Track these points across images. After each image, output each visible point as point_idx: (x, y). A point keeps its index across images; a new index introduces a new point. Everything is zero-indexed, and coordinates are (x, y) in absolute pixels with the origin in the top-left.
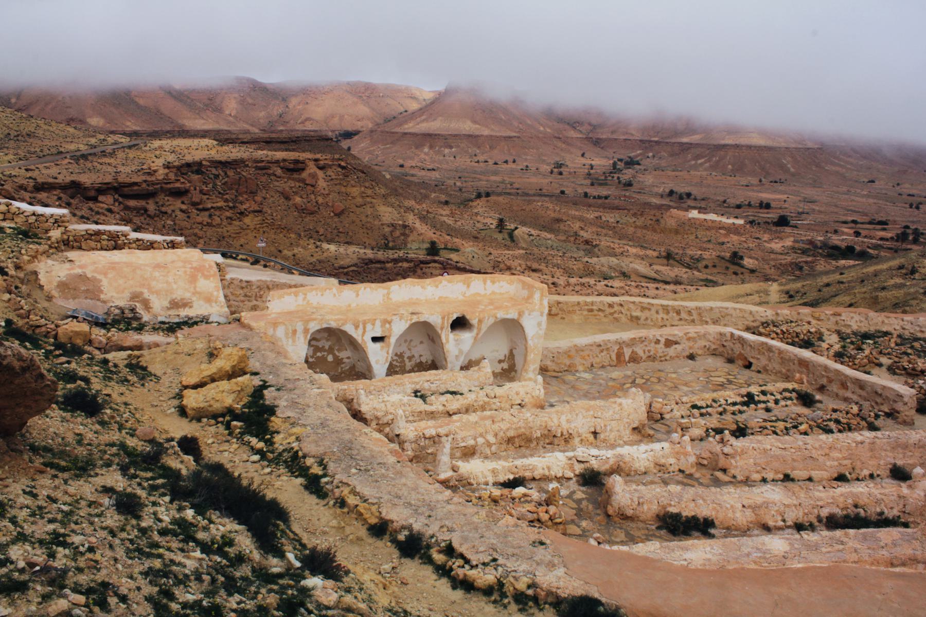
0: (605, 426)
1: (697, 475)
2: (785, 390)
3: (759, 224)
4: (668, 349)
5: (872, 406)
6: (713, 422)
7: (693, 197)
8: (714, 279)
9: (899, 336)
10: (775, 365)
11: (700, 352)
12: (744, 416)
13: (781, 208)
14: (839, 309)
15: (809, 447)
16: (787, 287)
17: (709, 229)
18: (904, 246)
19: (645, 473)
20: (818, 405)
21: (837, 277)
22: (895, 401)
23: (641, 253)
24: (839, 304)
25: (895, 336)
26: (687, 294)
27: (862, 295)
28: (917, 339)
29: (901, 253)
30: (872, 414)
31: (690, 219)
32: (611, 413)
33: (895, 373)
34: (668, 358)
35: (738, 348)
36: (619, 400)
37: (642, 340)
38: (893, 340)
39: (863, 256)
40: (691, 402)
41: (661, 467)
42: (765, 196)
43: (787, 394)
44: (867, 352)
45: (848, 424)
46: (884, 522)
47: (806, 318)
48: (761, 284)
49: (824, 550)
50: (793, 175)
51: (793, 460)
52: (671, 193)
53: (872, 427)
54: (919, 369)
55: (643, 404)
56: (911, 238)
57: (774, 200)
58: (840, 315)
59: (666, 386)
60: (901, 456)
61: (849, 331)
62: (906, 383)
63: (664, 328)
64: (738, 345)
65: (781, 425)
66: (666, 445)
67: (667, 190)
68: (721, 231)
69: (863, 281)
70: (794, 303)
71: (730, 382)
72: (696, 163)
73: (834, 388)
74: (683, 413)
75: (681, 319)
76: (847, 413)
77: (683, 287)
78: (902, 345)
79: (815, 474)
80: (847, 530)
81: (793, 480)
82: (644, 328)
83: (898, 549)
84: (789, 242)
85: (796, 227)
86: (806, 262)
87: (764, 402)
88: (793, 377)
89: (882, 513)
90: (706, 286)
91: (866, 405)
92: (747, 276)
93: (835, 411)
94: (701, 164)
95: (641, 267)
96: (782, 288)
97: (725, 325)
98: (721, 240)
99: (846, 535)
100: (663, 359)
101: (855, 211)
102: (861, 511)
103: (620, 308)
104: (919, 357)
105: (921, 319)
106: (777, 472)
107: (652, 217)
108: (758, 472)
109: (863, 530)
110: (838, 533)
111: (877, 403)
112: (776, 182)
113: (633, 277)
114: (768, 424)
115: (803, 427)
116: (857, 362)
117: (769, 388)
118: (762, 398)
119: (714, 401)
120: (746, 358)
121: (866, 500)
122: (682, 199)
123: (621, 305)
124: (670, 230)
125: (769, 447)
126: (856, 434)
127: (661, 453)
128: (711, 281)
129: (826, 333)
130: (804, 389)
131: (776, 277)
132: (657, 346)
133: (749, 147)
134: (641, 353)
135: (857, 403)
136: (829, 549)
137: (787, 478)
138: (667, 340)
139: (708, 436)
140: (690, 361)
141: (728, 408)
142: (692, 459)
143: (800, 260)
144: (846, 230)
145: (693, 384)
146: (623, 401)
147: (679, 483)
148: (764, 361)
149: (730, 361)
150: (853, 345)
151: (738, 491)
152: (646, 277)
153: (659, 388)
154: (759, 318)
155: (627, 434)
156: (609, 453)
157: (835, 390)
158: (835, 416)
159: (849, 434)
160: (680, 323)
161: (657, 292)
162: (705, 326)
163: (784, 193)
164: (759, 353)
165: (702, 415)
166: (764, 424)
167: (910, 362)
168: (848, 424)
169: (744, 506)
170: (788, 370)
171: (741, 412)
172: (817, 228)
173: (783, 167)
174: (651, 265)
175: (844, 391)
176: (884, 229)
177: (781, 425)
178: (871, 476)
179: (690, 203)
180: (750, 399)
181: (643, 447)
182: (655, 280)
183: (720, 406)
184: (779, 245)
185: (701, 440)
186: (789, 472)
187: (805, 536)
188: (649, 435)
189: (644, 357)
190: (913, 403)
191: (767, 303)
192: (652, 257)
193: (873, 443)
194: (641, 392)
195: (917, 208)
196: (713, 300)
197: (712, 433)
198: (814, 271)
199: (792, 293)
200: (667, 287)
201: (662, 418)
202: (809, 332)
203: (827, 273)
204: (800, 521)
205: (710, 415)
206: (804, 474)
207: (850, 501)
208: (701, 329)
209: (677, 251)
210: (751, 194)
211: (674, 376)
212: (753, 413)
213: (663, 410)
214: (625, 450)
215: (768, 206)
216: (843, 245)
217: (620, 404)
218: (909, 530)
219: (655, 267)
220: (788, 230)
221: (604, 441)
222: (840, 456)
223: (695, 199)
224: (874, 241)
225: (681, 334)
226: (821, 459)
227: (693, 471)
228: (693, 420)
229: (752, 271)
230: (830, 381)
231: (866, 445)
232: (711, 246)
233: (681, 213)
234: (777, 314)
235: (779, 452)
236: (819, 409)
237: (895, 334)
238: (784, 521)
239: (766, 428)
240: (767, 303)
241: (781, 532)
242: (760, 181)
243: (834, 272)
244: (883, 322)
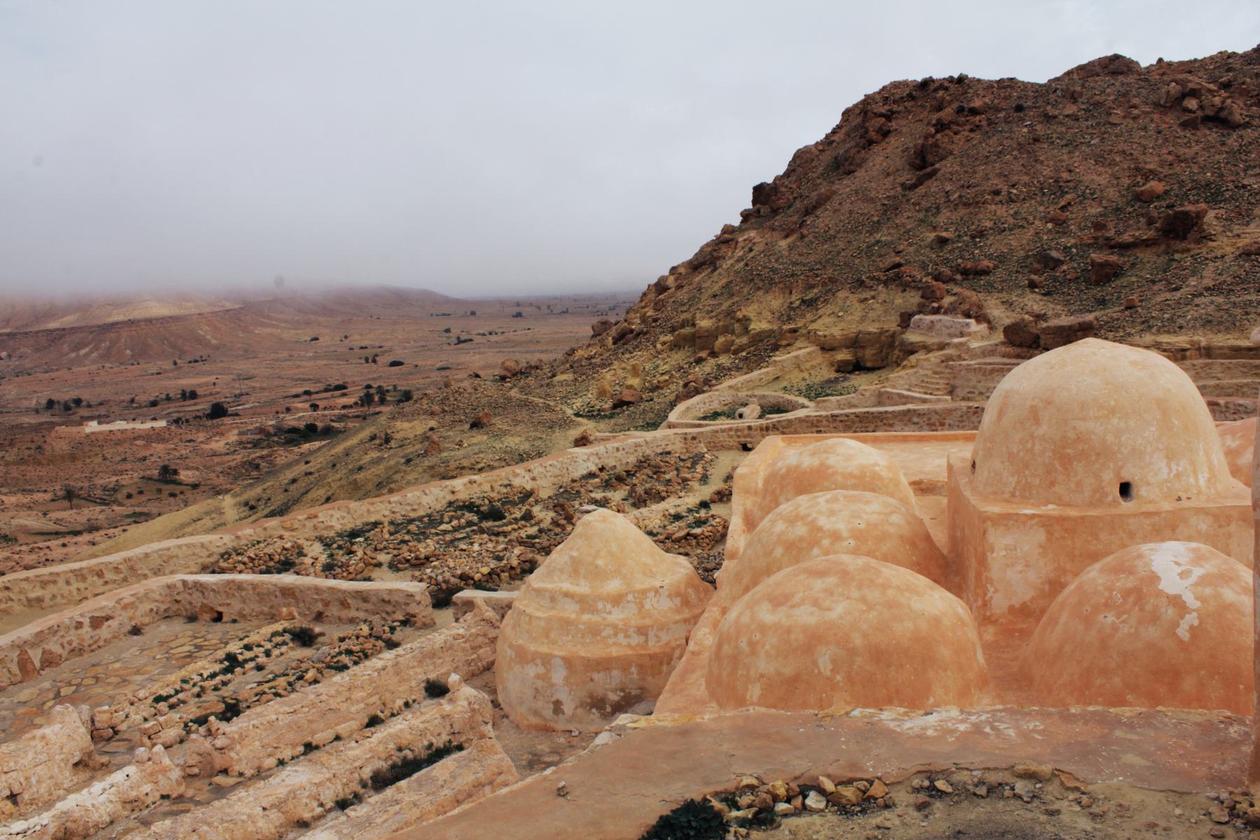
0: (27, 779)
1: (190, 793)
2: (275, 634)
3: (187, 421)
4: (98, 631)
5: (384, 619)
6: (192, 710)
7: (84, 403)
8: (145, 510)
9: (391, 523)
10: (252, 606)
11: (146, 620)
12: (231, 687)
13: (211, 394)
14: (313, 511)
15: (324, 697)
16: (245, 497)
17: (119, 443)
18: (372, 410)
19: (112, 822)
20: (321, 639)
21: (303, 468)
22: (407, 604)
23: (25, 501)
24: (314, 502)
25: (386, 524)
26: (109, 543)
27: (339, 483)
28: (411, 521)
29: (369, 421)
30: (386, 628)
31: (88, 436)
32: (31, 755)
33: (398, 570)
34: (101, 643)
35: (197, 599)
36: (38, 732)
37: (53, 631)
38: (385, 530)
39: (328, 432)
40: (151, 694)
41: (132, 804)
42: (187, 382)
43: (279, 639)
44: (360, 554)
45: (362, 651)
46: (437, 754)
47: (275, 533)
48: (210, 501)
49: (379, 821)
50: (217, 348)
51: (310, 722)
52: (51, 404)
53: (391, 645)
54: (422, 556)
55: (79, 723)
56: (376, 398)
57: (199, 386)
58: (316, 517)
59: (109, 684)
60: (431, 667)
61: (332, 534)
62: (414, 578)
63: (85, 603)
64: (197, 595)
65: (282, 681)
66: (131, 769)
67: (44, 402)
68: (138, 442)
69: (334, 465)
70: (259, 515)
71: (199, 648)
72: (78, 356)
73: (334, 611)
74: (146, 714)
75: (106, 583)
76: (358, 638)
77: (102, 532)
78: (396, 532)
79: (342, 729)
80: (398, 784)
81: (317, 747)
82: (53, 612)
83: (459, 780)
84: (233, 437)
85: (237, 415)
86: (262, 457)
87: (252, 659)
88: (280, 613)
89: (431, 745)
90: (136, 522)
91: (376, 619)
92: (189, 494)
93: (342, 640)
94: (87, 355)
95: (32, 521)
96: (238, 499)
97: (172, 572)
98: (140, 456)
99: (399, 790)
100: (95, 647)
101: (304, 380)
102: (407, 752)
103: (7, 593)
104: (419, 541)
105: (409, 495)
106: (294, 746)
107: (29, 445)
108: (270, 755)
109: (416, 776)
110: (389, 792)
111: (388, 613)
112: (196, 361)
113: (22, 538)
114: (265, 687)
115: (310, 675)
116: (351, 569)
117: (254, 638)
118: (248, 654)
119: (184, 681)
120: (212, 609)
121: (409, 737)
122: (71, 409)
123: (7, 588)
124: (63, 457)
125: (274, 717)
126: (374, 660)
127: (128, 783)
128: (141, 514)
129: (306, 544)
130: (298, 625)
131: (229, 486)
132: (79, 632)
133: (149, 321)
134: (57, 649)
135: (365, 621)
136: (385, 817)
137: (309, 748)
138: (92, 618)
139: (189, 732)
140: (135, 637)
141: (206, 684)
142: (176, 774)
143: (253, 456)
144: (300, 405)
145: (148, 668)
146: (46, 731)
147: (166, 815)
148: (237, 605)
149: (192, 619)
150: (343, 549)
151: (251, 791)
152: (42, 534)
153: (100, 690)
154: (215, 550)
155: (67, 777)
156: (46, 818)
157: (336, 613)
158: (344, 646)
159: (367, 663)
160: (107, 587)
161: (65, 550)
162: (144, 582)
163: (210, 373)
164: (228, 597)
165: (172, 707)
166: (261, 688)
167: (410, 551)
168: (362, 651)
169: (264, 809)
170: (271, 607)
171: (225, 684)
172: (264, 410)
173: (200, 340)
174: (45, 514)
175: (346, 611)
176: (344, 395)
177: (282, 681)
178: (407, 705)
179: (83, 412)
180: (232, 662)
181: (97, 786)
182: (57, 534)
183: (194, 685)
184: (222, 444)
185: (181, 742)
186: (309, 739)
187: (352, 814)
188: (103, 765)
189: (65, 654)
190: (428, 600)
191: (224, 524)
192: (45, 503)
193: (397, 664)
194: (71, 708)
195: (374, 361)
196: (145, 542)
197: (194, 727)
198: (274, 466)
199: (252, 503)
200: (79, 539)
201: (116, 733)
202: (284, 549)
203: (289, 466)
204: (341, 796)
205: (184, 702)
206: (330, 734)
207: (392, 746)
208: (139, 588)
209: (80, 484)
210: (166, 383)
211: (117, 665)
212: (242, 678)
213: (115, 721)
214: (69, 803)
215: (193, 395)
216: (301, 425)
217: (43, 737)
218: (464, 753)
219: (54, 515)
220: (227, 420)
221: (32, 801)
222: (364, 694)
223: (89, 406)
224: (336, 412)
225: (111, 604)
226: (343, 707)
227: (182, 789)
228: (161, 719)
229: (195, 486)
230: (327, 604)
231: (389, 669)
232: (128, 466)
233: (74, 430)
234: (238, 537)
235: (289, 718)
236: (323, 644)
237: (386, 521)
238: (321, 805)
239: (264, 693)
240: (224, 524)
241: (323, 821)
242: (175, 363)
243: (297, 462)
244: (368, 511)
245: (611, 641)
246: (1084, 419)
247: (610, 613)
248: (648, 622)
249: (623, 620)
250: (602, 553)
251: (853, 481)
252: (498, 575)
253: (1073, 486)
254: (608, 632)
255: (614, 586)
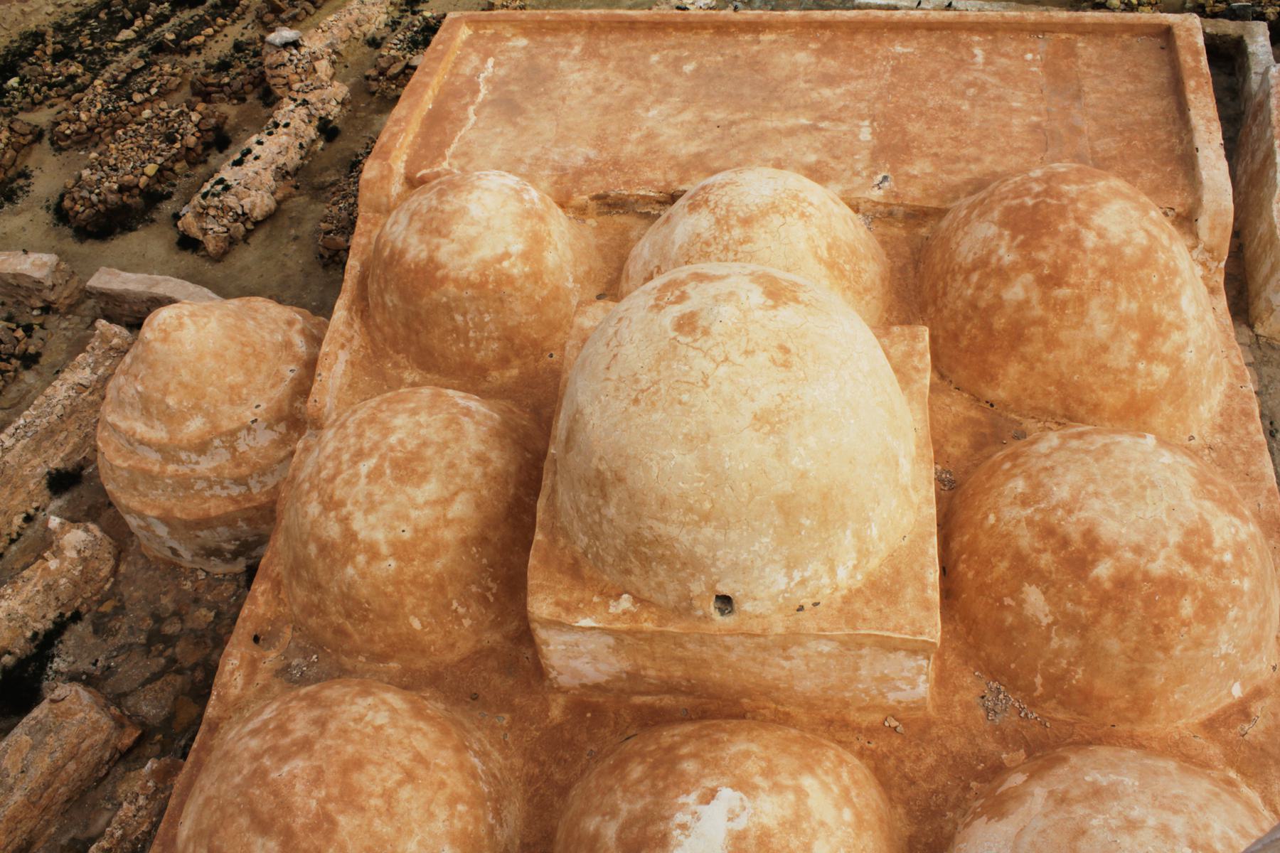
89: (36, 634)
245: (207, 494)
246: (665, 521)
247: (197, 463)
248: (244, 470)
249: (215, 469)
250: (172, 387)
251: (470, 292)
252: (172, 170)
253: (653, 584)
254: (200, 485)
255: (195, 426)
